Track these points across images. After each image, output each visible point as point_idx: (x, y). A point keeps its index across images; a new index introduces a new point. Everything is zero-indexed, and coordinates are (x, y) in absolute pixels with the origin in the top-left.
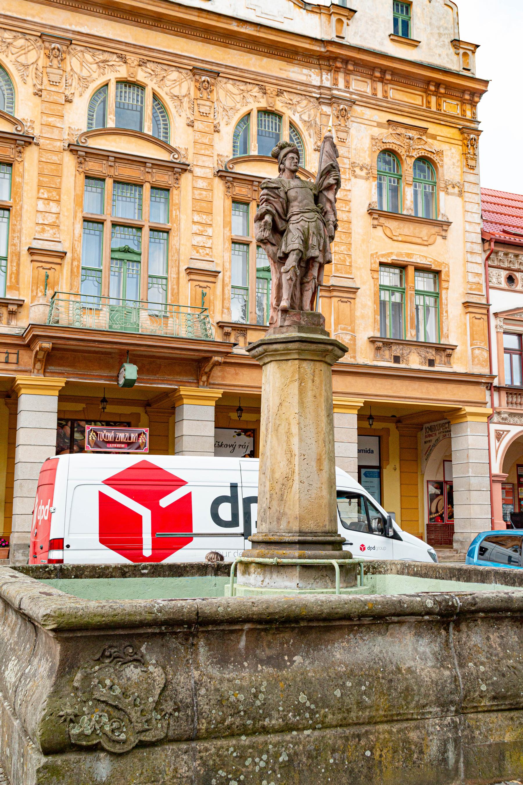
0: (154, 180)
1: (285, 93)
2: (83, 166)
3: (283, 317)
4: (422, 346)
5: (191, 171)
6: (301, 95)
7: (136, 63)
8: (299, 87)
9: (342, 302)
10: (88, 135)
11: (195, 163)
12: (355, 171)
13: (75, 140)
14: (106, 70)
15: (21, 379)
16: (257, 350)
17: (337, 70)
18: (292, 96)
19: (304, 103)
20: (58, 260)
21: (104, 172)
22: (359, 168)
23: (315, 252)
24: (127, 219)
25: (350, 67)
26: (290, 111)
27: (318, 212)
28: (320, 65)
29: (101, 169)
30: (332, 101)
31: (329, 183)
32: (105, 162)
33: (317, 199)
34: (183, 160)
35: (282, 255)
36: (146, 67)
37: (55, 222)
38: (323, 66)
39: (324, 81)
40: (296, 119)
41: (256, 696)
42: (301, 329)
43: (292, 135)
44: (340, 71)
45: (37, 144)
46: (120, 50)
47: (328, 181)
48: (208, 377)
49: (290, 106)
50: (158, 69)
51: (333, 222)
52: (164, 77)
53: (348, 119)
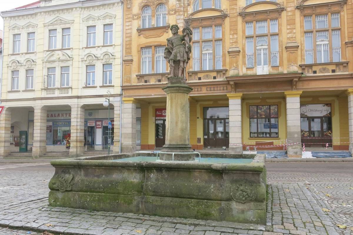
4: (155, 75)
5: (286, 10)
11: (287, 6)
15: (228, 95)
20: (238, 54)
34: (282, 7)
37: (236, 41)
41: (91, 183)
45: (229, 16)
48: (296, 86)
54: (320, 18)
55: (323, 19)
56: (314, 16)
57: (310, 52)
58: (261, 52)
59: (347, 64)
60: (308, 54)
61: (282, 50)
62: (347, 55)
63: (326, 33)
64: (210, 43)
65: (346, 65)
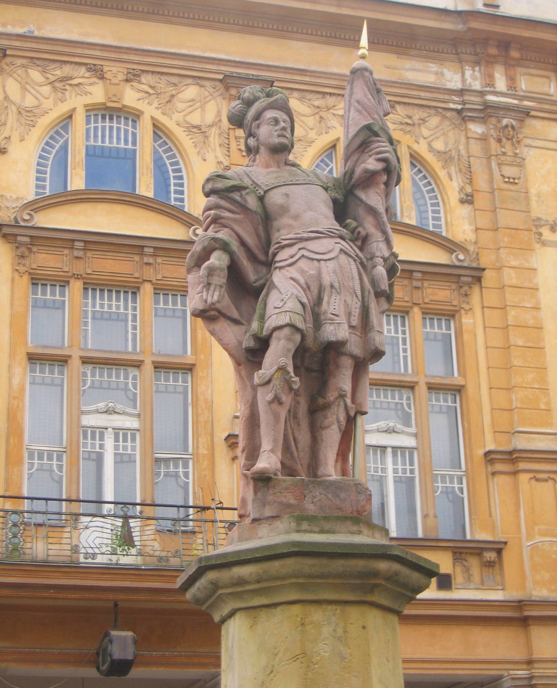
0: (159, 277)
1: (398, 107)
2: (27, 262)
3: (259, 494)
6: (429, 107)
7: (121, 77)
8: (423, 94)
9: (537, 480)
10: (38, 205)
12: (540, 234)
13: (12, 217)
14: (67, 93)
16: (198, 584)
17: (491, 61)
18: (410, 111)
19: (434, 121)
21: (66, 269)
22: (548, 227)
23: (337, 330)
24: (105, 351)
25: (515, 54)
26: (408, 136)
27: (342, 238)
28: (457, 54)
29: (59, 265)
30: (487, 112)
31: (366, 171)
32: (66, 252)
33: (342, 210)
35: (251, 344)
36: (140, 82)
38: (464, 57)
39: (469, 80)
40: (422, 149)
42: (303, 519)
43: (417, 178)
44: (496, 62)
46: (93, 60)
47: (363, 166)
49: (408, 128)
50: (162, 83)
51: (385, 260)
52: (173, 96)
53: (518, 142)
54: (114, 303)
55: (118, 307)
56: (77, 286)
57: (50, 458)
58: (101, 446)
59: (499, 552)
60: (41, 469)
61: (212, 449)
62: (497, 513)
63: (405, 397)
64: (126, 378)
65: (491, 556)
